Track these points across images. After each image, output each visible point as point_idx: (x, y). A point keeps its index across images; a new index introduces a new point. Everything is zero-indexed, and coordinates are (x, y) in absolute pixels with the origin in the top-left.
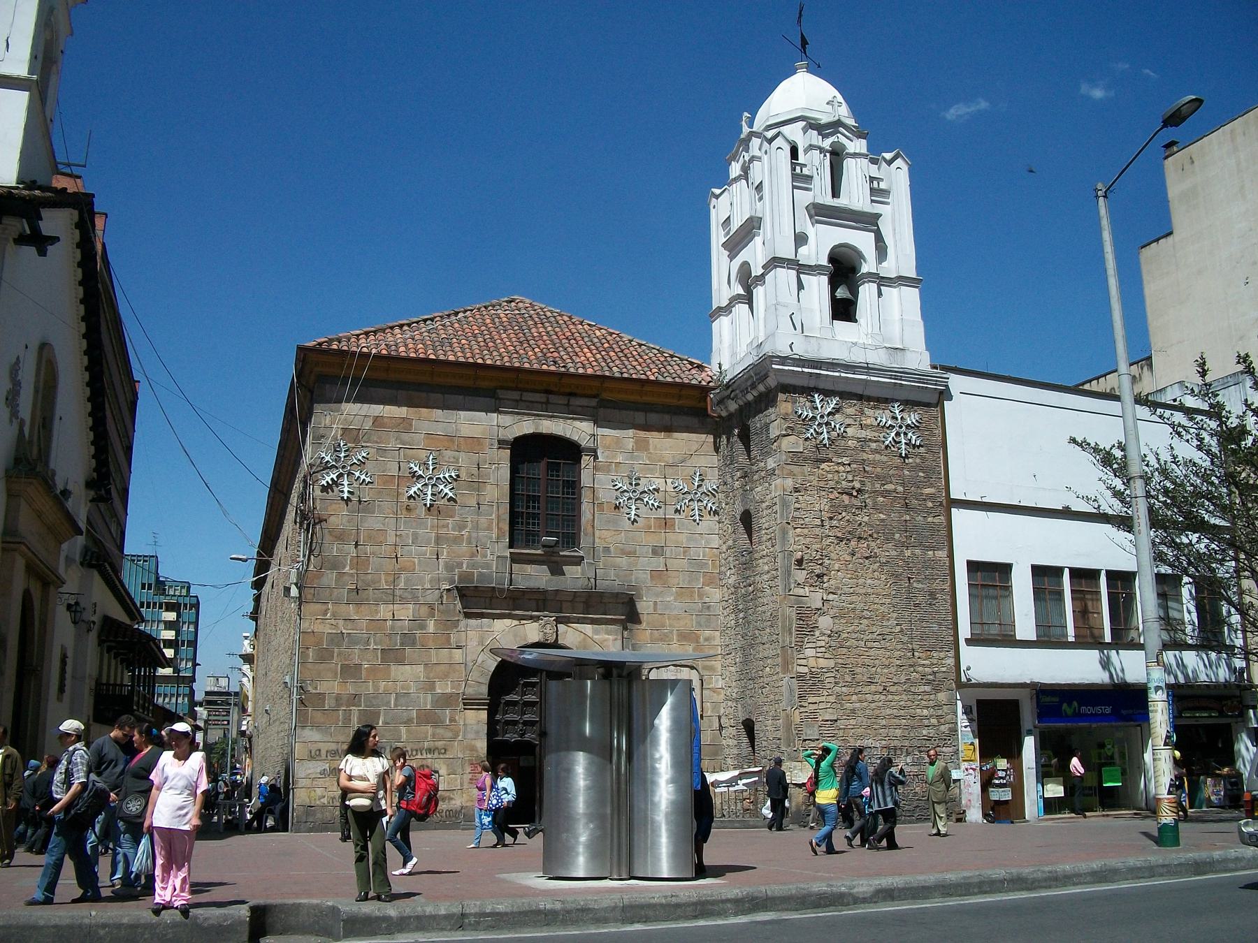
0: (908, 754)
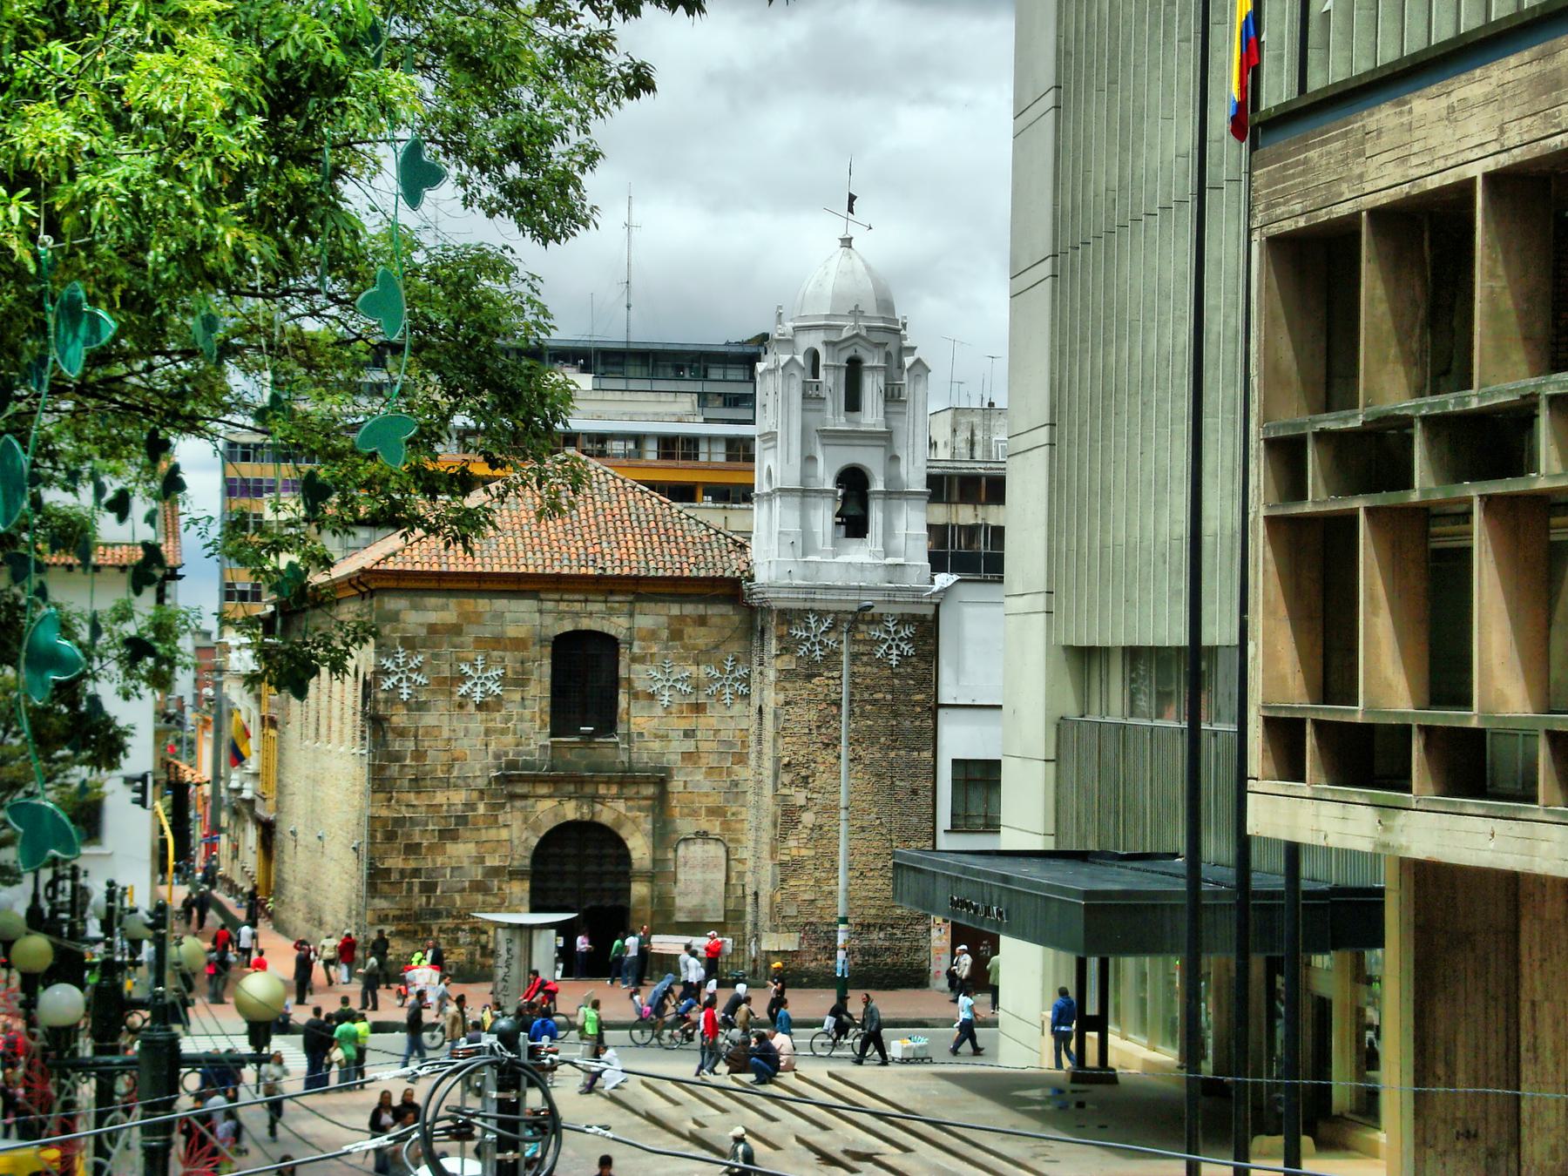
0: (881, 929)
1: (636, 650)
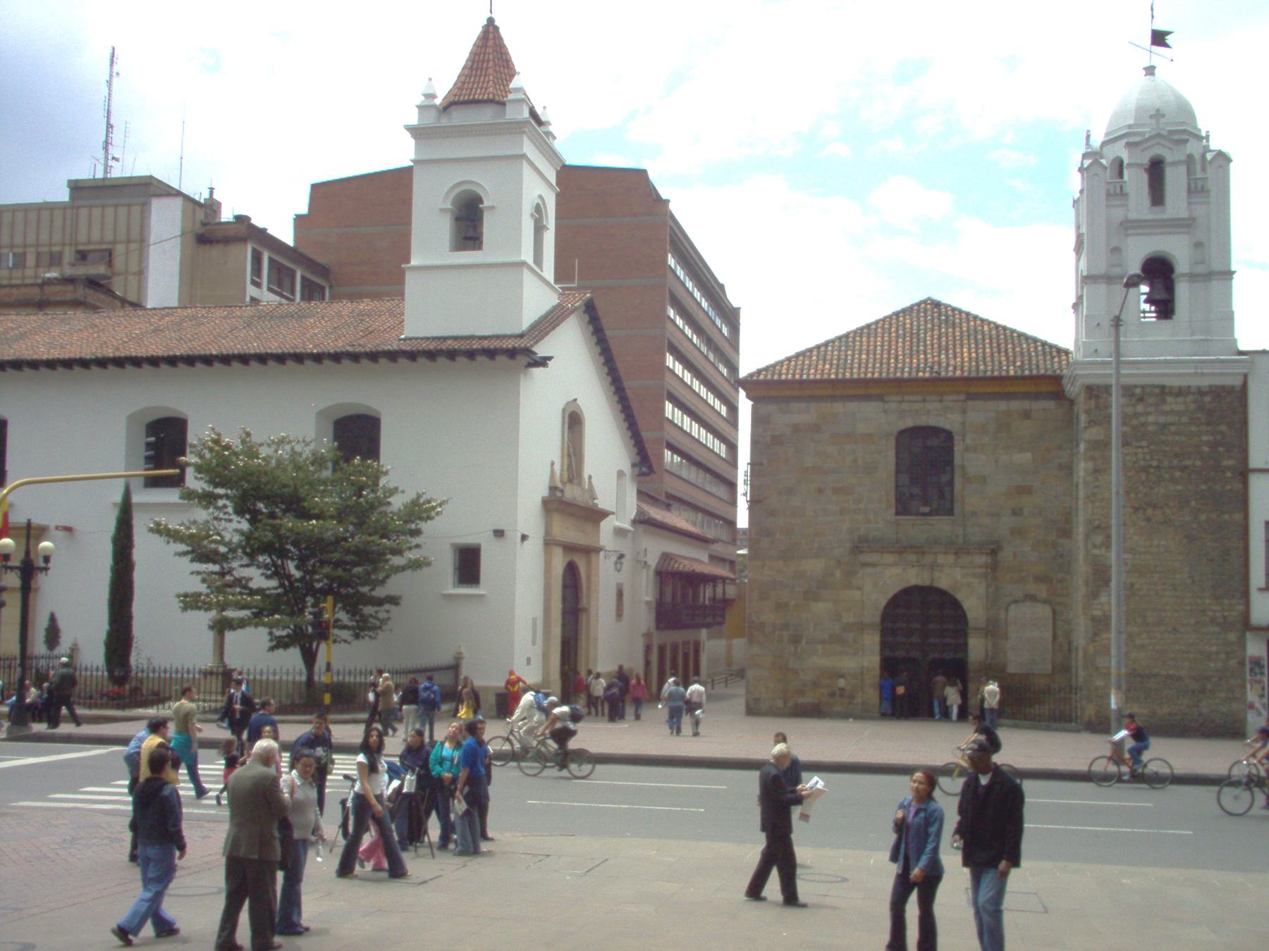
1: (968, 441)
